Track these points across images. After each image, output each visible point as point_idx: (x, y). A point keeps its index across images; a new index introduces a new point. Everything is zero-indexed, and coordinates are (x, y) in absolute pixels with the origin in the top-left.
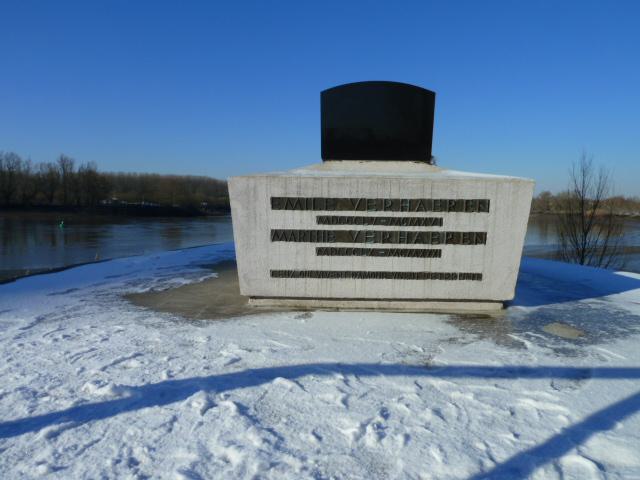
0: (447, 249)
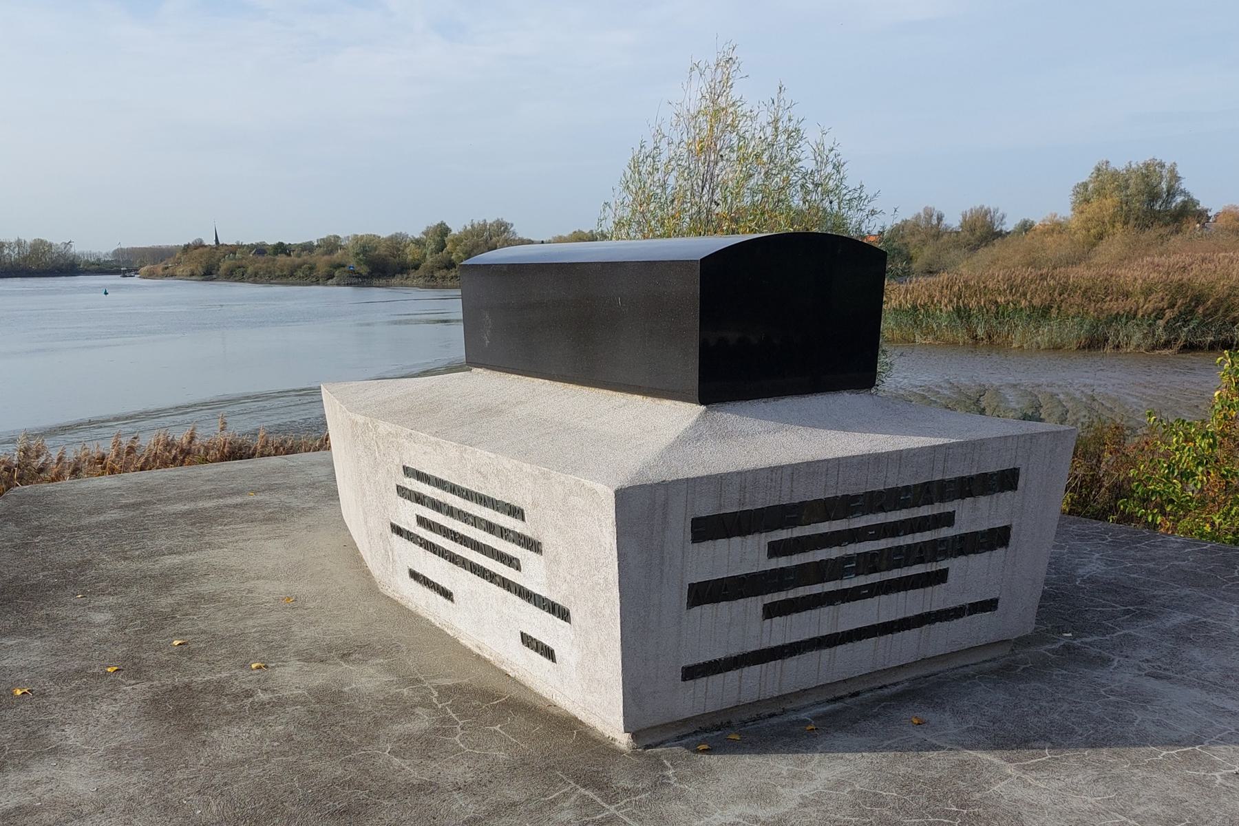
0: (954, 565)
